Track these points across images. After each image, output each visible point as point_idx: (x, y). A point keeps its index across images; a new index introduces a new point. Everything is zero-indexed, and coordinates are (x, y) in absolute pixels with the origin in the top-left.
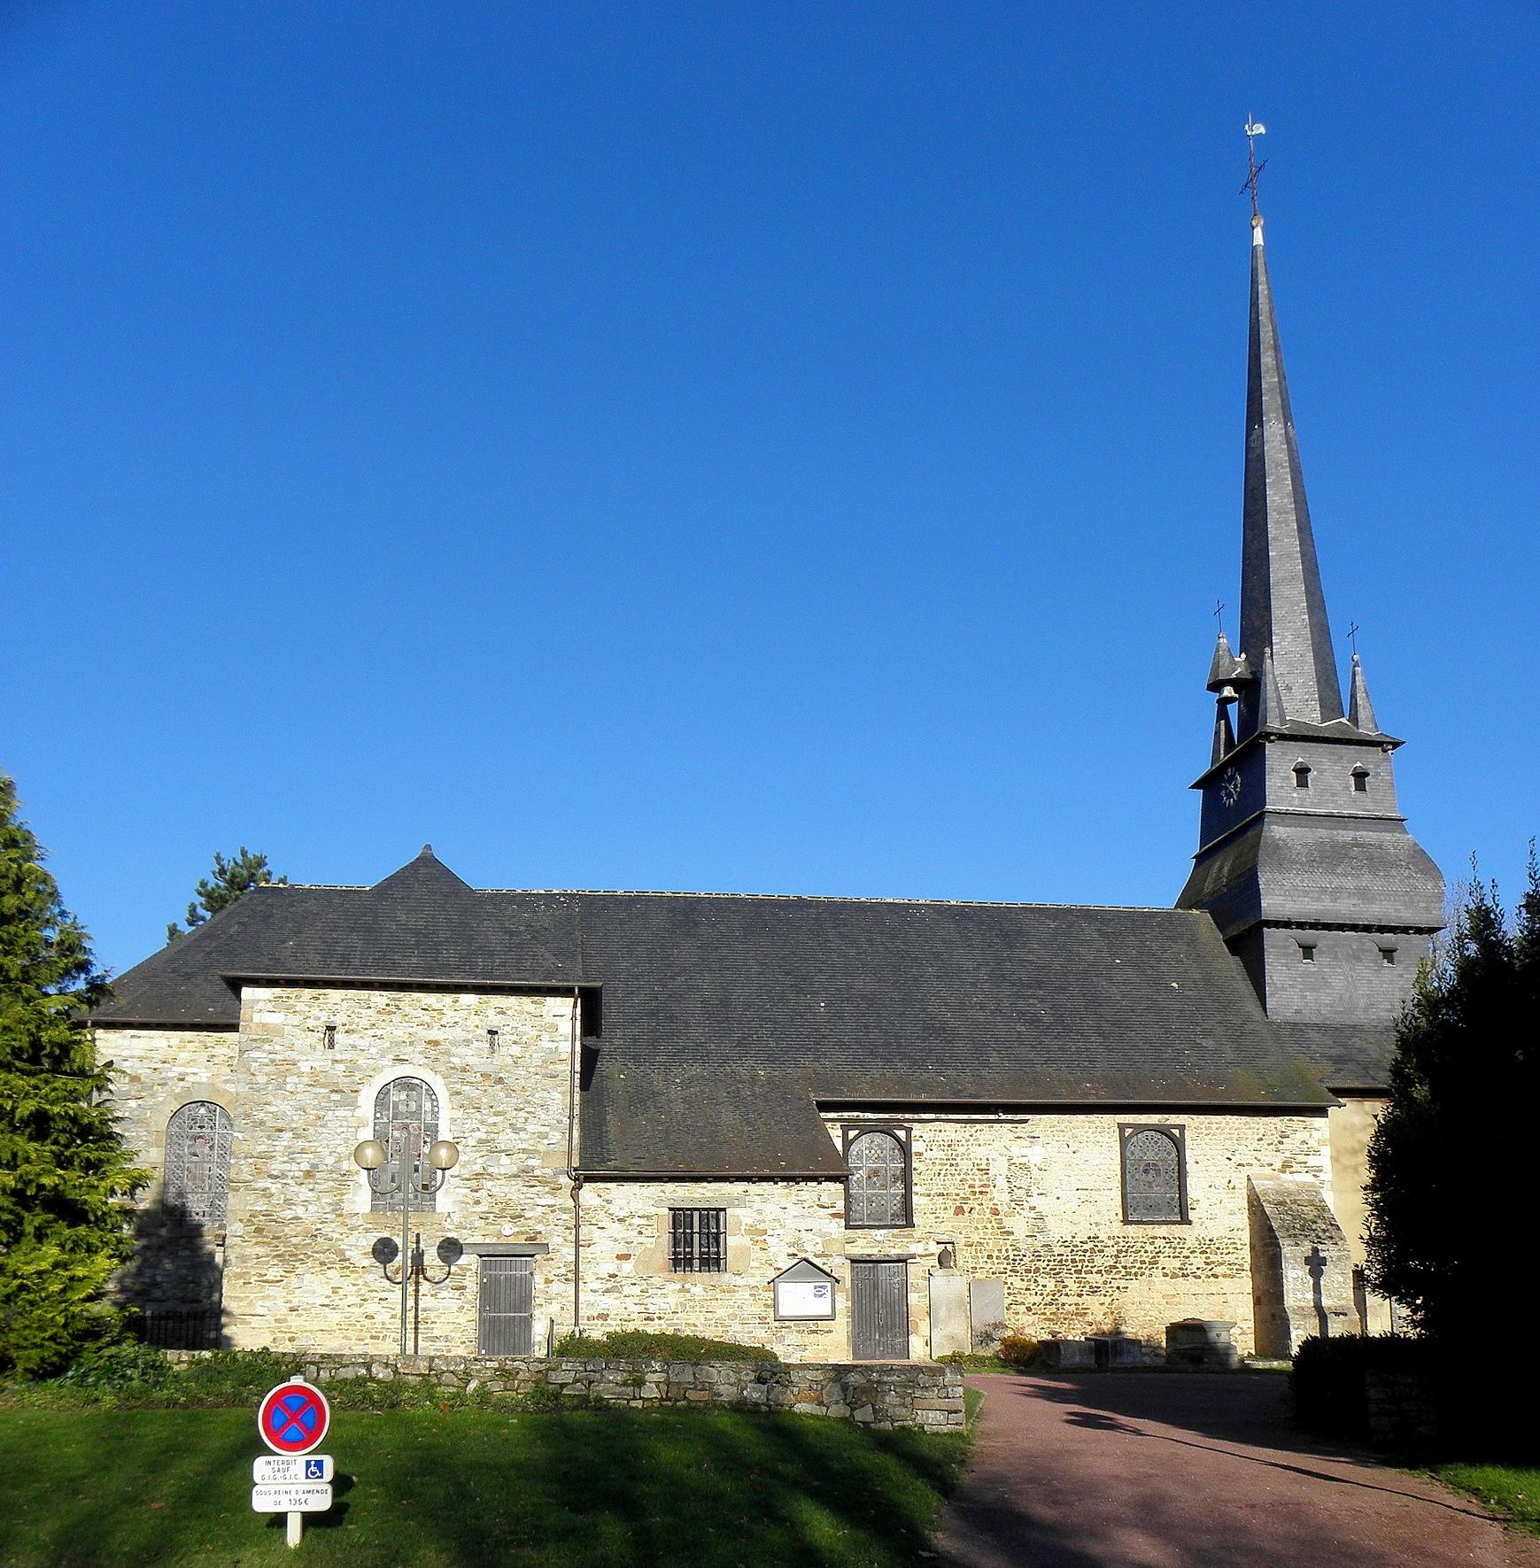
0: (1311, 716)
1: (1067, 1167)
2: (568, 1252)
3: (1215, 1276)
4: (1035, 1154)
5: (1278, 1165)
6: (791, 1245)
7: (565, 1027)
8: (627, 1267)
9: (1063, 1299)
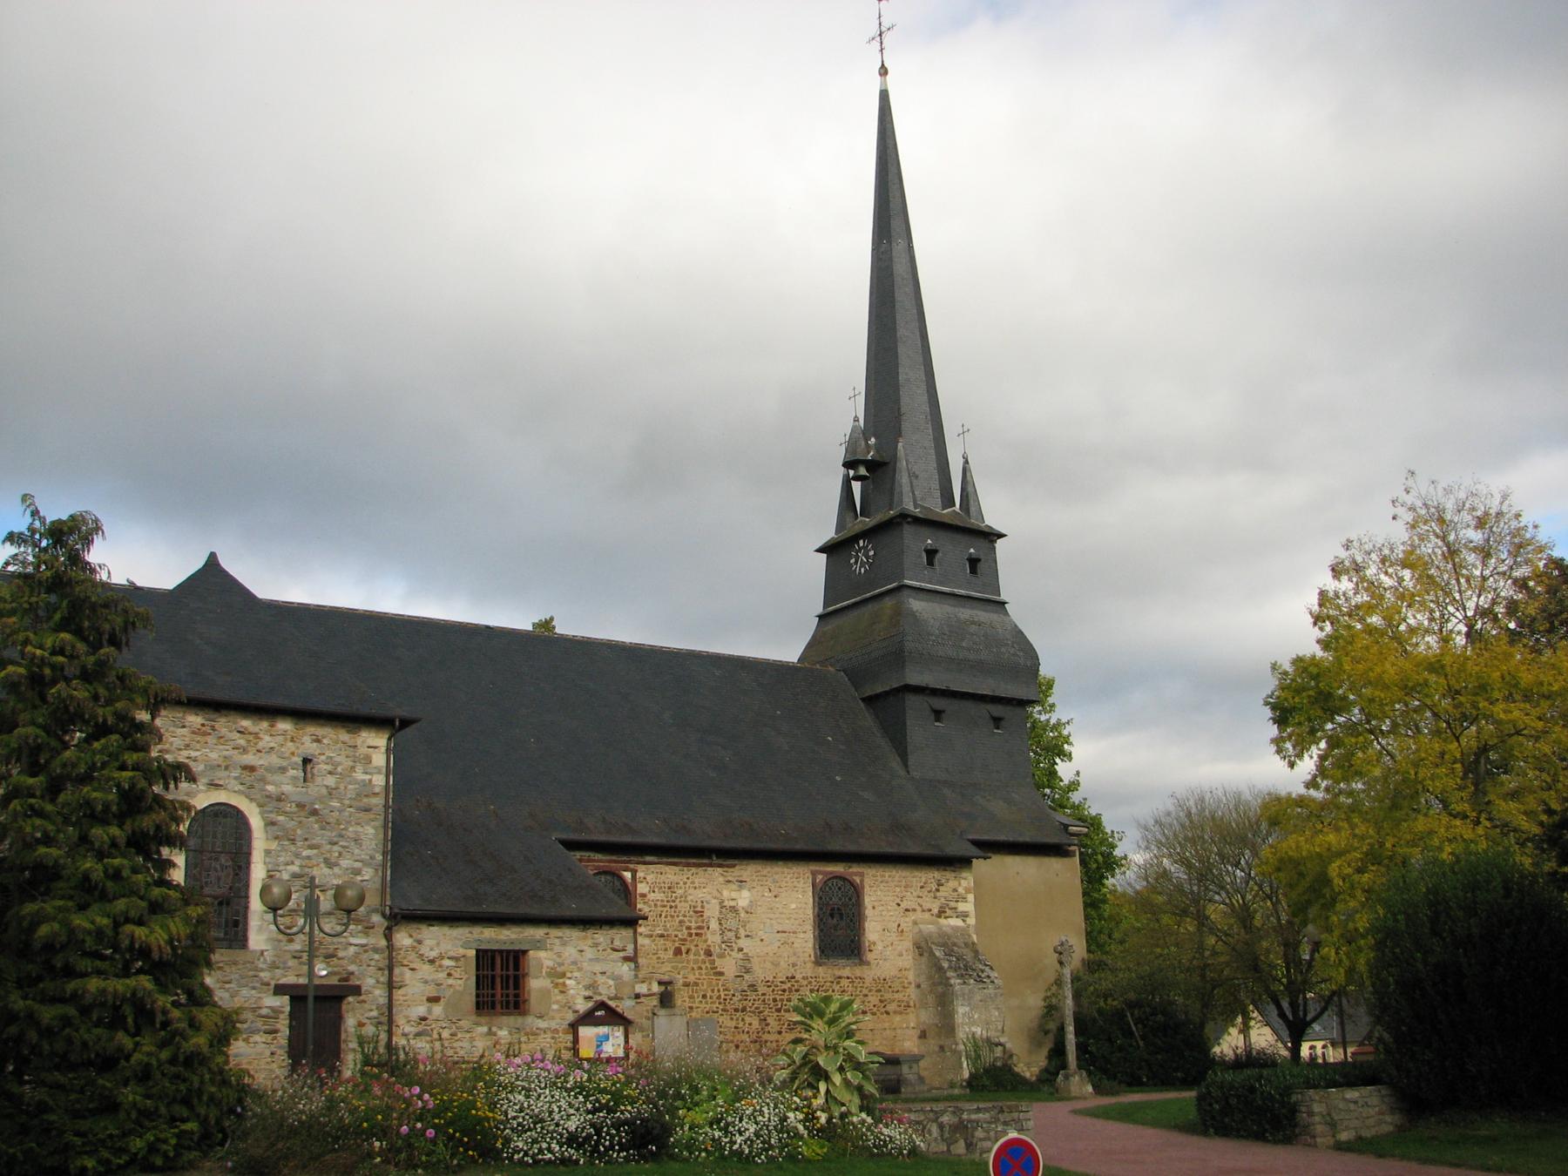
1: (768, 912)
2: (380, 994)
4: (743, 898)
5: (936, 911)
6: (587, 988)
7: (379, 759)
8: (438, 1010)
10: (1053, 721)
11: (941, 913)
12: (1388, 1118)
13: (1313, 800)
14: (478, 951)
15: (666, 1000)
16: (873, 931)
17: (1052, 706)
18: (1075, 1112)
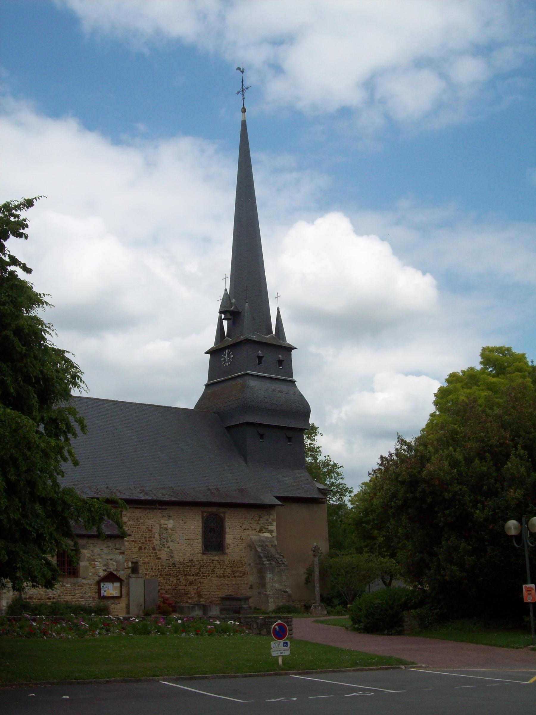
3: (235, 577)
4: (170, 524)
5: (258, 530)
6: (104, 566)
11: (261, 531)
15: (135, 569)
16: (229, 539)
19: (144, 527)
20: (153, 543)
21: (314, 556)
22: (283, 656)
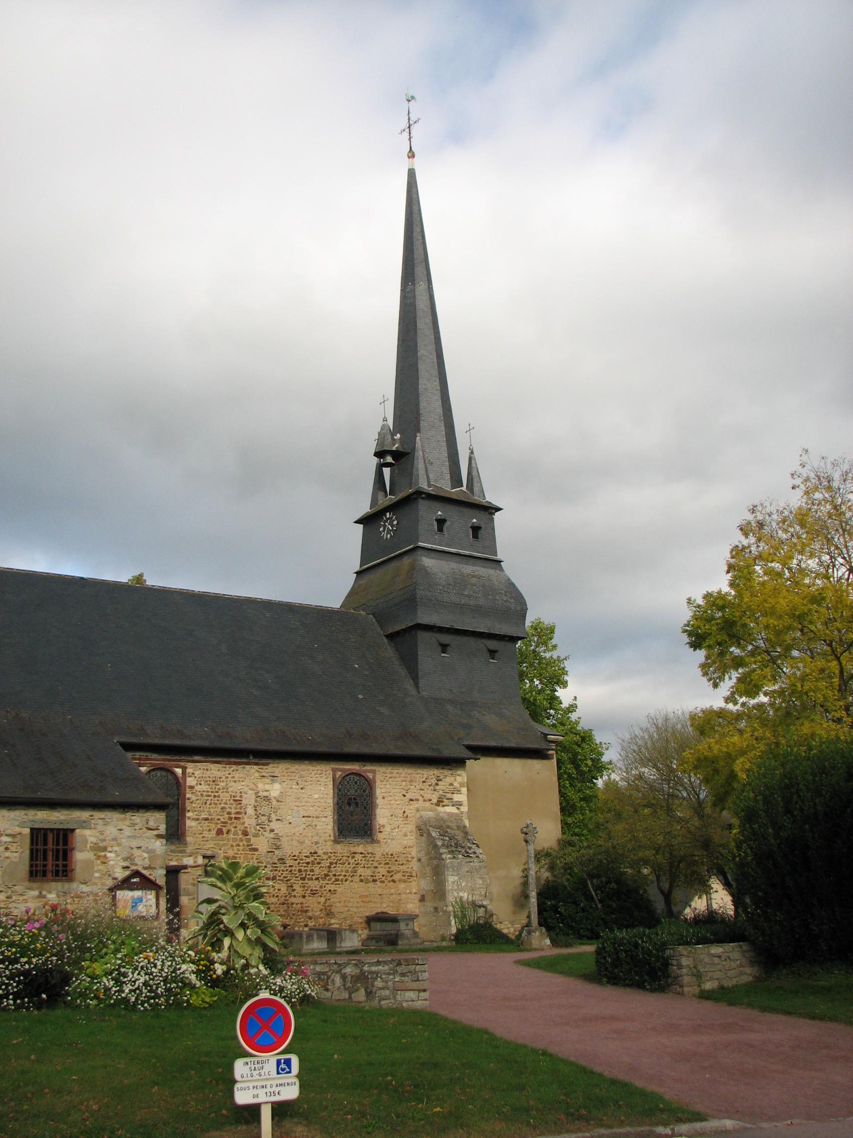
0: (445, 486)
1: (294, 802)
4: (275, 790)
5: (435, 801)
6: (125, 859)
9: (292, 900)
10: (555, 657)
11: (439, 802)
12: (748, 970)
13: (731, 712)
14: (32, 829)
16: (383, 816)
17: (555, 647)
18: (519, 962)
19: (228, 795)
20: (244, 823)
21: (526, 841)
22: (273, 1103)
